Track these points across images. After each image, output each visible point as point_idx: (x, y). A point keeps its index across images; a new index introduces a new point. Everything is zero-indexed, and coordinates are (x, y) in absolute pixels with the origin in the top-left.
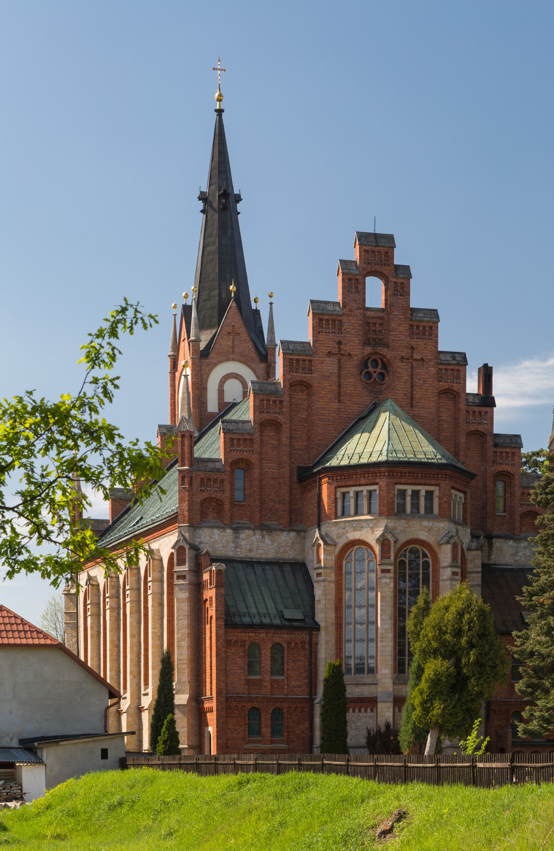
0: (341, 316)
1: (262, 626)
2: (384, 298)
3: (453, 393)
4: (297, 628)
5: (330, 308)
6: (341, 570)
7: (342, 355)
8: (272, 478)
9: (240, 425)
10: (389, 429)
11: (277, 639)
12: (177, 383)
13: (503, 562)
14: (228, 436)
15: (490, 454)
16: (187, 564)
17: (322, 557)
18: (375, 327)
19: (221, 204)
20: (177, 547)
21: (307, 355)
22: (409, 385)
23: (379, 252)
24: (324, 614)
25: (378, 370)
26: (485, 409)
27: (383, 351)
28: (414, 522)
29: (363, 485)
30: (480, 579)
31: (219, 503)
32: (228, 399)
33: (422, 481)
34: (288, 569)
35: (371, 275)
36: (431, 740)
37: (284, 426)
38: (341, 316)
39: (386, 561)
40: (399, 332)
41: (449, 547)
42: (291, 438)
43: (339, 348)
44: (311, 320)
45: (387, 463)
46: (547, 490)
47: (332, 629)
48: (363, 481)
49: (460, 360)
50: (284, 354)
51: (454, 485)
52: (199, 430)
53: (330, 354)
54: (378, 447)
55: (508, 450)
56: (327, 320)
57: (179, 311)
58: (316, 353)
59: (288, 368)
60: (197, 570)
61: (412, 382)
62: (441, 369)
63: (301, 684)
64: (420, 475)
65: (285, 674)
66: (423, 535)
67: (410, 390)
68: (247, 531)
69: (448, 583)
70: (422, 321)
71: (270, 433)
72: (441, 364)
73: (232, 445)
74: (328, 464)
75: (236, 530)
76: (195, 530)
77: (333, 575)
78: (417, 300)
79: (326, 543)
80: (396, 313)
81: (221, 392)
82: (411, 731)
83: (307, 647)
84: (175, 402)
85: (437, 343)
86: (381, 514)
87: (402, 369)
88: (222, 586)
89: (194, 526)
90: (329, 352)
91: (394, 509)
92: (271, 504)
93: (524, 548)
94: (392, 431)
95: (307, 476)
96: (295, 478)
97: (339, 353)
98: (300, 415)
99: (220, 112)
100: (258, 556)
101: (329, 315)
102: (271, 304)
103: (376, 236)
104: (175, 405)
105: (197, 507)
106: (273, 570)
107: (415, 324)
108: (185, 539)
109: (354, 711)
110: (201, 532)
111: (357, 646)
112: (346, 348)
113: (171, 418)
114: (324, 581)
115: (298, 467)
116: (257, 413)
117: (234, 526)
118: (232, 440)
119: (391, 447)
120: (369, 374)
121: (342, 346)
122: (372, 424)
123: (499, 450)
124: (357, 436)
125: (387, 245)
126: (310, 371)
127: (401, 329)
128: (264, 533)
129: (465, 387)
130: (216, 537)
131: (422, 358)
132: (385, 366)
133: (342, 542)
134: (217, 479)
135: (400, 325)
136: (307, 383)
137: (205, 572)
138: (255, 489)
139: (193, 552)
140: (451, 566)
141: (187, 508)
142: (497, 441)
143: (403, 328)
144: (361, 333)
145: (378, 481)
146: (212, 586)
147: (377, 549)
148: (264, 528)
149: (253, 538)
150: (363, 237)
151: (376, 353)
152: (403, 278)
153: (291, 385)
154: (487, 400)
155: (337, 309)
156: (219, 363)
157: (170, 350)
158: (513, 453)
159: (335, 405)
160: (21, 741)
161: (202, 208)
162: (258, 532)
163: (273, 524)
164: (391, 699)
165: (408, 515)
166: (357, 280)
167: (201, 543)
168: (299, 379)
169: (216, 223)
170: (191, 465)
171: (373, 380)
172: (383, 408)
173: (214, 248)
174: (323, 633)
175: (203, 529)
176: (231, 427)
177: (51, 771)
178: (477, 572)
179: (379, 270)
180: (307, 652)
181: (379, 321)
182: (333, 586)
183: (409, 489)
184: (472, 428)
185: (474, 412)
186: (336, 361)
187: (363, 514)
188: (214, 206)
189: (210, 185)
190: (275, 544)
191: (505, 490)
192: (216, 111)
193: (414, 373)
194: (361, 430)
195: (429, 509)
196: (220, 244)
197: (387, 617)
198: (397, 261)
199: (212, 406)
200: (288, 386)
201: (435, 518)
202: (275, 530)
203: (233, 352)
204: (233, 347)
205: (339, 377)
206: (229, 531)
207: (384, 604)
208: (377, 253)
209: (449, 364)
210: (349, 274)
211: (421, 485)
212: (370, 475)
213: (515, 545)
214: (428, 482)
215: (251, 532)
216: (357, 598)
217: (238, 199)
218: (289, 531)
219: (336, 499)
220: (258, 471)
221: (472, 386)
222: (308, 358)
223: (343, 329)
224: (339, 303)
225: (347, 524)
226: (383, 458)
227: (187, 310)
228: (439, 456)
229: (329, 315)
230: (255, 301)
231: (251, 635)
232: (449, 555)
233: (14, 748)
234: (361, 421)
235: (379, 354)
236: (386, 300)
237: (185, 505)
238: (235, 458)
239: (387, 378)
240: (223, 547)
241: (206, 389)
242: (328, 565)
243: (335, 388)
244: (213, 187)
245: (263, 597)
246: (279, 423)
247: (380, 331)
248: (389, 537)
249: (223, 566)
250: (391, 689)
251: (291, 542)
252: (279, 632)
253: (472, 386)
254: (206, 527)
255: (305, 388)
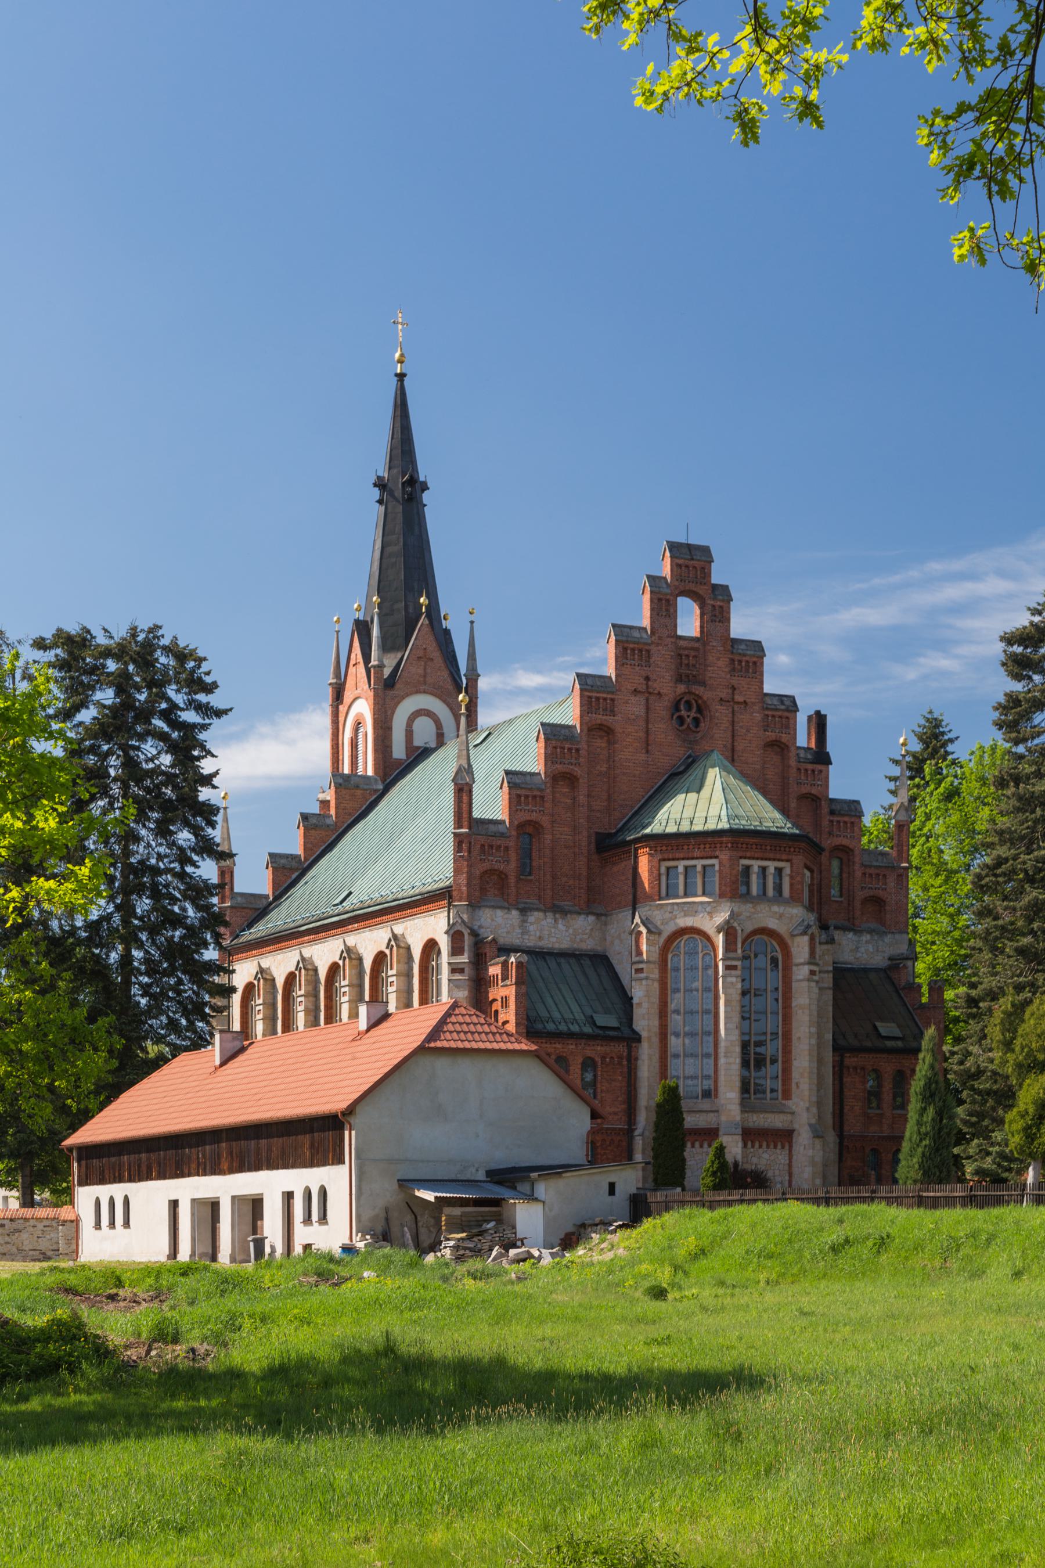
0: (649, 644)
1: (571, 1035)
2: (698, 624)
3: (780, 747)
4: (612, 1039)
5: (636, 634)
6: (666, 965)
7: (650, 693)
8: (566, 847)
9: (528, 777)
10: (723, 790)
11: (589, 1053)
12: (341, 719)
13: (841, 960)
14: (514, 792)
15: (825, 823)
16: (466, 955)
17: (644, 948)
18: (689, 658)
19: (403, 494)
20: (452, 932)
21: (608, 693)
22: (729, 734)
23: (694, 567)
24: (645, 1021)
25: (693, 714)
26: (819, 767)
27: (699, 690)
28: (762, 906)
29: (697, 858)
30: (831, 980)
31: (502, 877)
32: (418, 742)
33: (772, 856)
34: (587, 962)
35: (692, 598)
36: (1035, 1173)
37: (581, 780)
38: (649, 644)
39: (731, 955)
40: (717, 667)
41: (806, 938)
42: (589, 796)
43: (647, 684)
44: (613, 648)
45: (731, 832)
46: (999, 871)
47: (656, 1040)
48: (697, 853)
49: (789, 705)
50: (581, 690)
51: (808, 863)
52: (383, 781)
53: (636, 692)
54: (714, 811)
55: (846, 819)
56: (633, 650)
57: (348, 627)
58: (620, 690)
59: (585, 708)
60: (479, 962)
61: (733, 731)
62: (767, 715)
63: (616, 1110)
64: (768, 848)
65: (599, 1097)
66: (772, 924)
67: (730, 740)
68: (536, 913)
69: (805, 984)
70: (745, 655)
71: (564, 789)
72: (767, 709)
73: (519, 803)
74: (648, 831)
75: (524, 911)
76: (474, 910)
77: (657, 971)
78: (740, 626)
79: (649, 931)
80: (714, 644)
81: (409, 733)
82: (917, 1166)
83: (625, 1063)
84: (337, 744)
85: (762, 683)
86: (722, 895)
87: (721, 713)
88: (523, 983)
89: (474, 906)
90: (635, 690)
91: (736, 888)
92: (564, 879)
93: (867, 942)
94: (728, 791)
95: (612, 845)
96: (593, 846)
97: (647, 692)
98: (598, 768)
99: (401, 377)
100: (550, 946)
101: (634, 643)
102: (472, 622)
103: (689, 546)
104: (338, 748)
105: (476, 882)
106: (569, 963)
107: (737, 658)
108: (463, 921)
109: (693, 1146)
110: (481, 913)
111: (687, 1062)
112: (655, 685)
113: (333, 764)
114: (647, 978)
115: (597, 833)
116: (549, 763)
117: (521, 906)
118: (519, 796)
119: (730, 810)
120: (681, 720)
121: (650, 683)
122: (698, 781)
123: (836, 818)
124: (681, 797)
125: (703, 558)
126: (613, 713)
127: (720, 663)
128: (557, 916)
129: (795, 738)
130: (499, 920)
131: (745, 702)
132: (700, 710)
133: (668, 930)
134: (500, 846)
135: (718, 659)
136: (608, 727)
137: (493, 965)
138: (546, 860)
139: (472, 939)
140: (809, 963)
141: (465, 882)
142: (833, 807)
143: (723, 662)
144: (673, 667)
145: (717, 853)
146: (508, 982)
147: (720, 940)
148: (556, 910)
149: (544, 923)
150: (674, 547)
151: (690, 693)
152: (723, 601)
153: (590, 730)
154: (821, 757)
155: (645, 636)
156: (407, 695)
157: (331, 676)
158: (852, 823)
159: (642, 757)
160: (490, 1173)
161: (378, 498)
162: (550, 915)
163: (566, 904)
164: (740, 1131)
165: (754, 897)
166: (668, 601)
167: (480, 927)
168: (599, 722)
169: (400, 518)
170: (470, 828)
171: (685, 727)
172: (708, 763)
173: (398, 548)
174: (645, 1045)
175: (483, 909)
176: (517, 781)
177: (551, 1210)
178: (827, 972)
179: (695, 589)
180: (625, 1070)
181: (693, 653)
182: (656, 985)
183: (756, 865)
184: (804, 790)
185: (806, 770)
186: (642, 699)
187: (696, 896)
188: (396, 494)
189: (390, 468)
190: (571, 931)
191: (841, 869)
192: (396, 375)
193: (736, 719)
194: (685, 789)
195: (779, 888)
196: (405, 544)
197: (733, 1026)
198: (716, 579)
199: (399, 752)
200: (585, 730)
201: (787, 902)
202: (571, 912)
203: (425, 683)
204: (425, 676)
205: (647, 721)
206: (515, 913)
207: (729, 1009)
208: (692, 570)
209: (777, 710)
210: (659, 593)
211: (770, 859)
212: (708, 846)
213: (855, 938)
214: (778, 856)
215: (541, 915)
216: (687, 1002)
217: (424, 487)
218: (587, 914)
219: (660, 875)
220: (550, 837)
221: (803, 738)
222: (609, 696)
223: (652, 661)
224: (645, 629)
225: (676, 907)
226: (724, 825)
227: (362, 628)
228: (789, 825)
229: (634, 643)
230: (445, 619)
231: (558, 1046)
232: (807, 949)
233: (480, 1181)
234: (681, 775)
235: (694, 694)
236: (702, 627)
237: (463, 879)
238: (522, 820)
239: (702, 725)
240: (508, 933)
241: (390, 728)
242: (651, 959)
243: (642, 734)
244: (395, 471)
245: (564, 998)
246: (575, 777)
247: (694, 666)
248: (735, 924)
249: (525, 958)
250: (738, 1118)
251: (589, 928)
252: (591, 1043)
253: (803, 738)
254: (487, 906)
255: (604, 734)
